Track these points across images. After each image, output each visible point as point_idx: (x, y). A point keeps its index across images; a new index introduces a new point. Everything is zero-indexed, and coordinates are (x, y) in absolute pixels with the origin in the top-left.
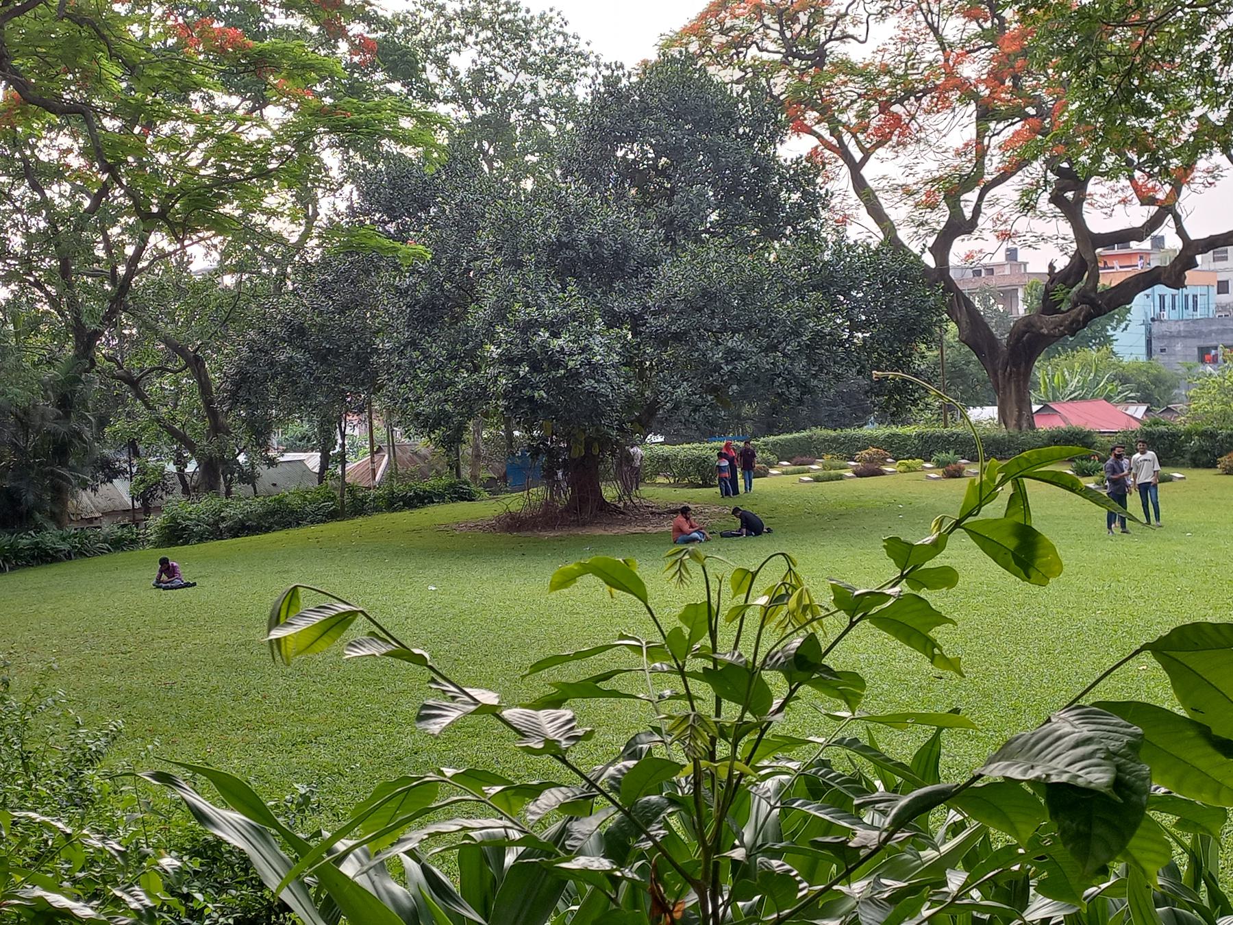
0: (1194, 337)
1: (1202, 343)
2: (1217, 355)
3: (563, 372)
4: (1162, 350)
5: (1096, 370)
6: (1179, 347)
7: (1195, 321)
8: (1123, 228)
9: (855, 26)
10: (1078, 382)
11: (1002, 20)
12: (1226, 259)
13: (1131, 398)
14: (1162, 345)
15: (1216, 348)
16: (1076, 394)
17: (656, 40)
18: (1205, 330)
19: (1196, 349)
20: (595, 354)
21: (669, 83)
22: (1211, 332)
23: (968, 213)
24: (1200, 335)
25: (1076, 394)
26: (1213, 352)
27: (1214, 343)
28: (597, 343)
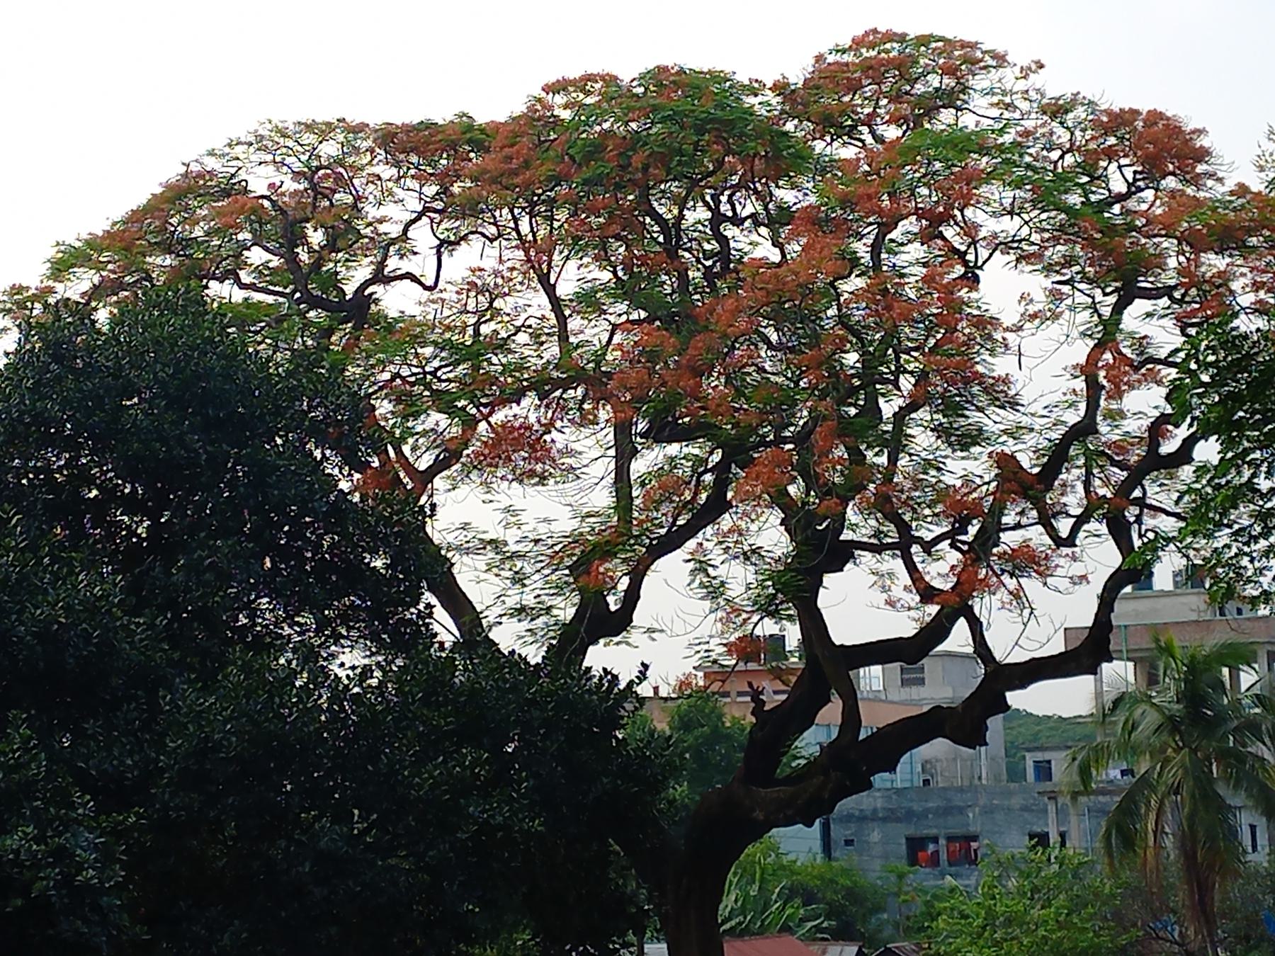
0: (898, 820)
1: (912, 831)
2: (937, 852)
3: (19, 902)
4: (849, 843)
5: (762, 880)
6: (875, 836)
7: (899, 792)
8: (874, 640)
9: (401, 258)
10: (736, 901)
11: (207, 234)
12: (921, 682)
13: (823, 931)
14: (848, 833)
15: (935, 840)
16: (733, 923)
17: (52, 252)
18: (916, 807)
19: (904, 841)
20: (80, 868)
21: (172, 346)
22: (927, 811)
23: (613, 603)
24: (909, 816)
25: (733, 923)
26: (931, 848)
27: (934, 831)
28: (85, 844)
